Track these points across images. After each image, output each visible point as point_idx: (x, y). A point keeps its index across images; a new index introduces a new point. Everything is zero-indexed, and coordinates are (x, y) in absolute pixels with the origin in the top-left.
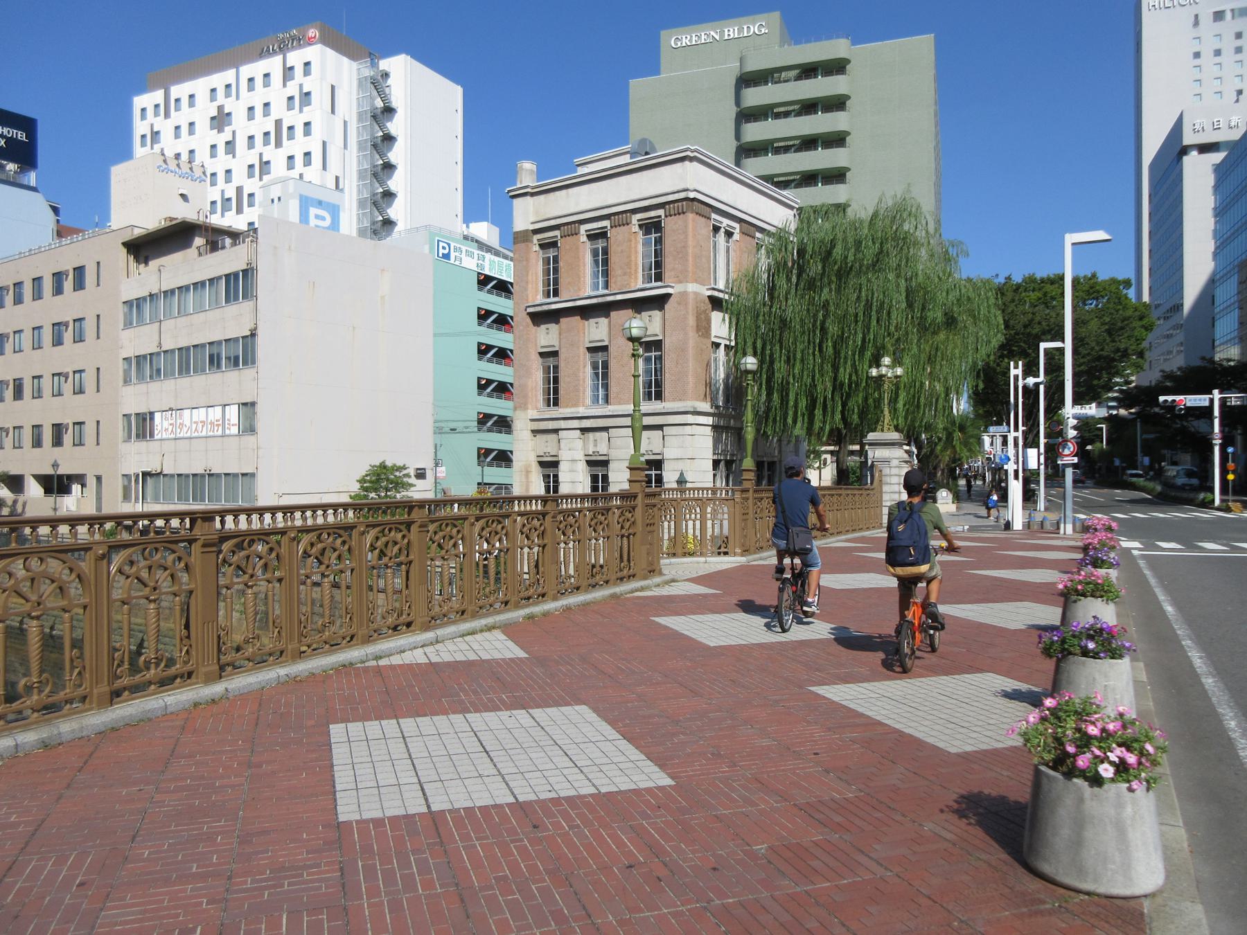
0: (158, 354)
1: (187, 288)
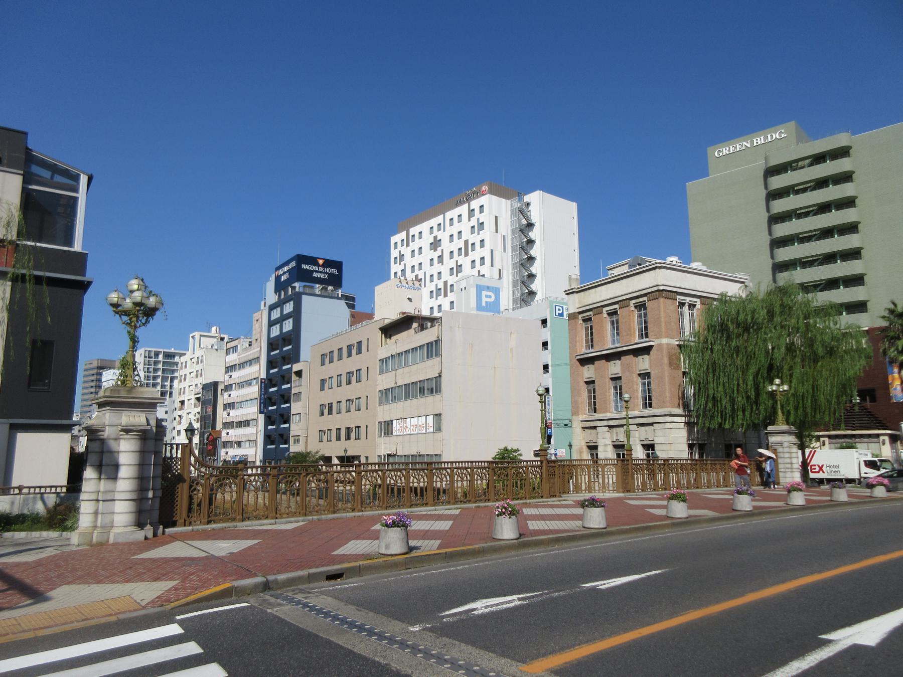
0: (395, 388)
1: (409, 351)
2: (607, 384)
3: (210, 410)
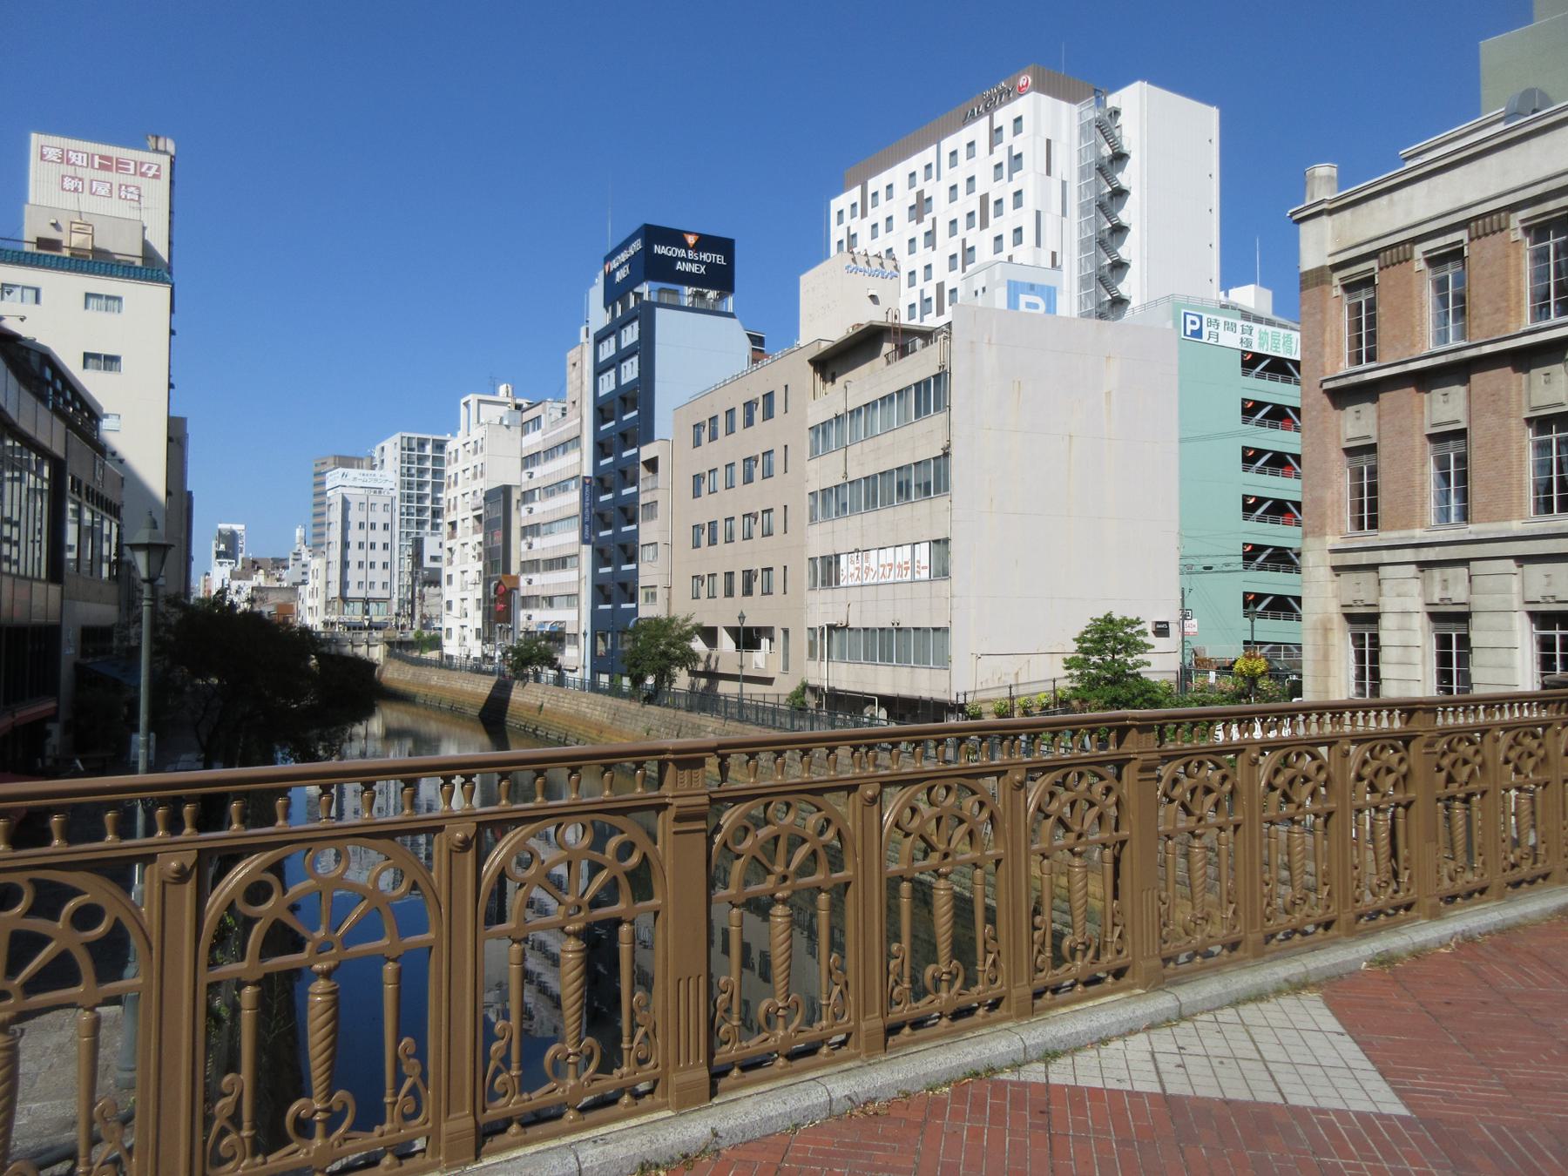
0: (844, 485)
1: (874, 404)
2: (1418, 451)
3: (498, 539)
